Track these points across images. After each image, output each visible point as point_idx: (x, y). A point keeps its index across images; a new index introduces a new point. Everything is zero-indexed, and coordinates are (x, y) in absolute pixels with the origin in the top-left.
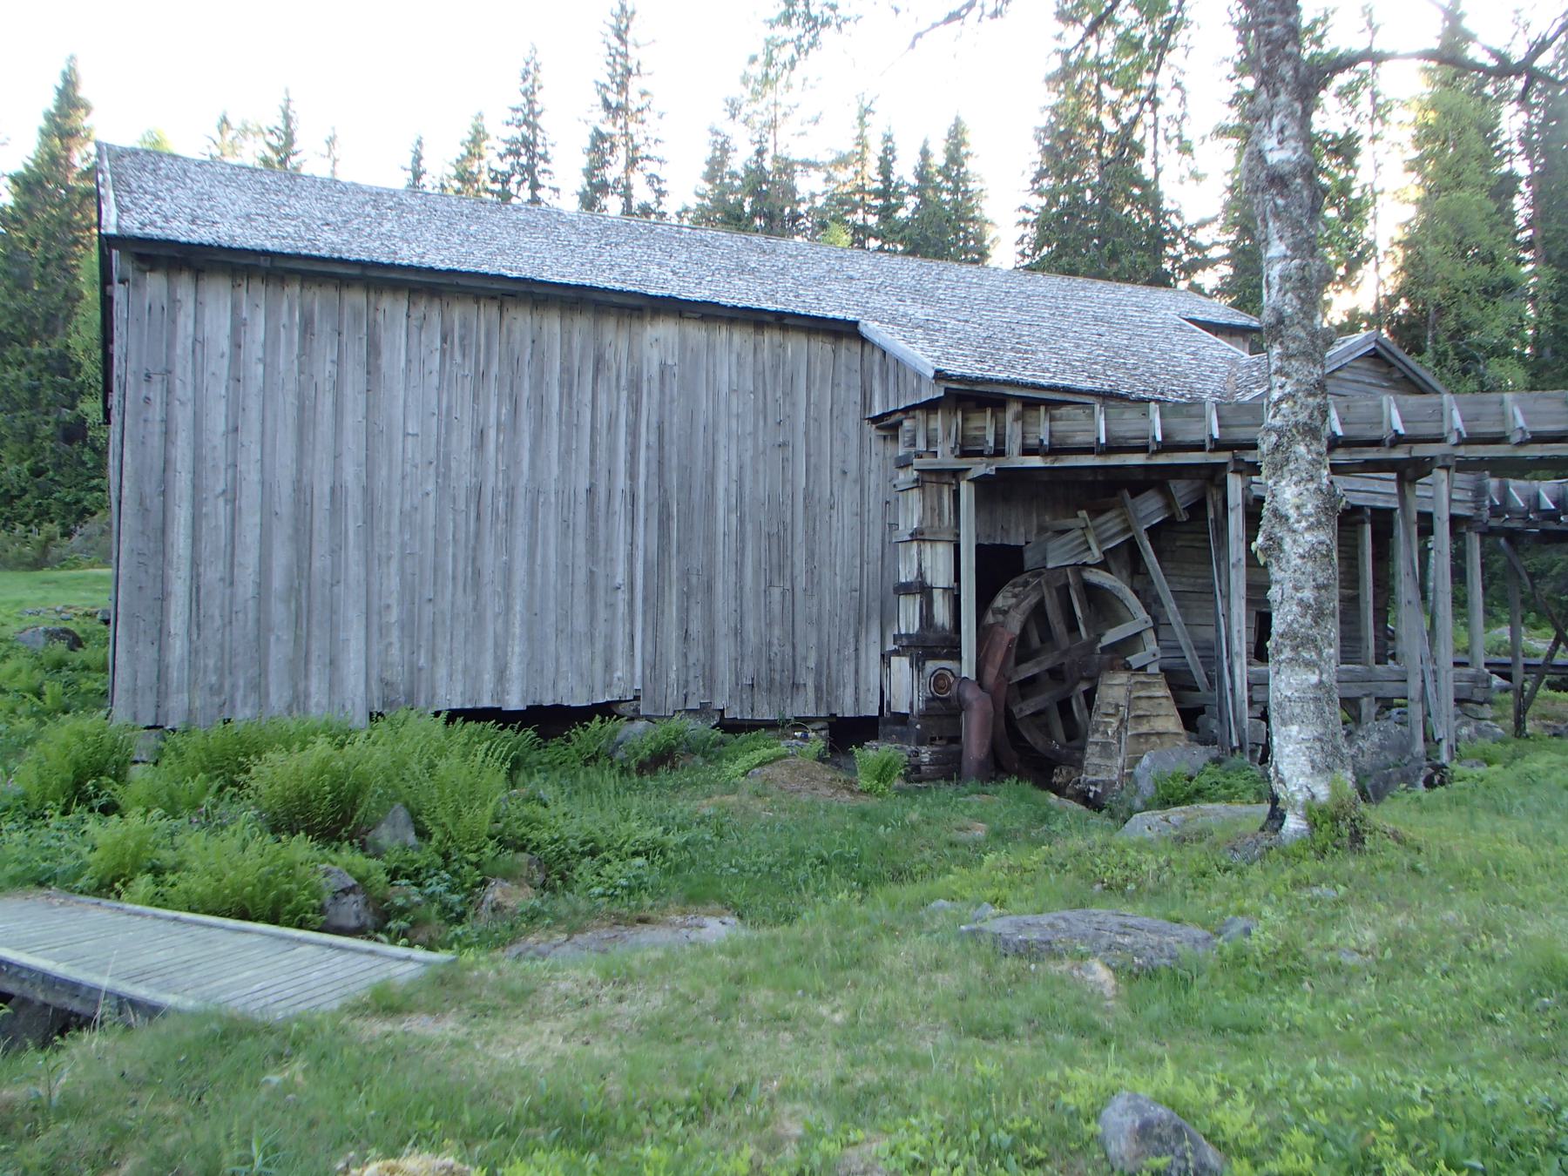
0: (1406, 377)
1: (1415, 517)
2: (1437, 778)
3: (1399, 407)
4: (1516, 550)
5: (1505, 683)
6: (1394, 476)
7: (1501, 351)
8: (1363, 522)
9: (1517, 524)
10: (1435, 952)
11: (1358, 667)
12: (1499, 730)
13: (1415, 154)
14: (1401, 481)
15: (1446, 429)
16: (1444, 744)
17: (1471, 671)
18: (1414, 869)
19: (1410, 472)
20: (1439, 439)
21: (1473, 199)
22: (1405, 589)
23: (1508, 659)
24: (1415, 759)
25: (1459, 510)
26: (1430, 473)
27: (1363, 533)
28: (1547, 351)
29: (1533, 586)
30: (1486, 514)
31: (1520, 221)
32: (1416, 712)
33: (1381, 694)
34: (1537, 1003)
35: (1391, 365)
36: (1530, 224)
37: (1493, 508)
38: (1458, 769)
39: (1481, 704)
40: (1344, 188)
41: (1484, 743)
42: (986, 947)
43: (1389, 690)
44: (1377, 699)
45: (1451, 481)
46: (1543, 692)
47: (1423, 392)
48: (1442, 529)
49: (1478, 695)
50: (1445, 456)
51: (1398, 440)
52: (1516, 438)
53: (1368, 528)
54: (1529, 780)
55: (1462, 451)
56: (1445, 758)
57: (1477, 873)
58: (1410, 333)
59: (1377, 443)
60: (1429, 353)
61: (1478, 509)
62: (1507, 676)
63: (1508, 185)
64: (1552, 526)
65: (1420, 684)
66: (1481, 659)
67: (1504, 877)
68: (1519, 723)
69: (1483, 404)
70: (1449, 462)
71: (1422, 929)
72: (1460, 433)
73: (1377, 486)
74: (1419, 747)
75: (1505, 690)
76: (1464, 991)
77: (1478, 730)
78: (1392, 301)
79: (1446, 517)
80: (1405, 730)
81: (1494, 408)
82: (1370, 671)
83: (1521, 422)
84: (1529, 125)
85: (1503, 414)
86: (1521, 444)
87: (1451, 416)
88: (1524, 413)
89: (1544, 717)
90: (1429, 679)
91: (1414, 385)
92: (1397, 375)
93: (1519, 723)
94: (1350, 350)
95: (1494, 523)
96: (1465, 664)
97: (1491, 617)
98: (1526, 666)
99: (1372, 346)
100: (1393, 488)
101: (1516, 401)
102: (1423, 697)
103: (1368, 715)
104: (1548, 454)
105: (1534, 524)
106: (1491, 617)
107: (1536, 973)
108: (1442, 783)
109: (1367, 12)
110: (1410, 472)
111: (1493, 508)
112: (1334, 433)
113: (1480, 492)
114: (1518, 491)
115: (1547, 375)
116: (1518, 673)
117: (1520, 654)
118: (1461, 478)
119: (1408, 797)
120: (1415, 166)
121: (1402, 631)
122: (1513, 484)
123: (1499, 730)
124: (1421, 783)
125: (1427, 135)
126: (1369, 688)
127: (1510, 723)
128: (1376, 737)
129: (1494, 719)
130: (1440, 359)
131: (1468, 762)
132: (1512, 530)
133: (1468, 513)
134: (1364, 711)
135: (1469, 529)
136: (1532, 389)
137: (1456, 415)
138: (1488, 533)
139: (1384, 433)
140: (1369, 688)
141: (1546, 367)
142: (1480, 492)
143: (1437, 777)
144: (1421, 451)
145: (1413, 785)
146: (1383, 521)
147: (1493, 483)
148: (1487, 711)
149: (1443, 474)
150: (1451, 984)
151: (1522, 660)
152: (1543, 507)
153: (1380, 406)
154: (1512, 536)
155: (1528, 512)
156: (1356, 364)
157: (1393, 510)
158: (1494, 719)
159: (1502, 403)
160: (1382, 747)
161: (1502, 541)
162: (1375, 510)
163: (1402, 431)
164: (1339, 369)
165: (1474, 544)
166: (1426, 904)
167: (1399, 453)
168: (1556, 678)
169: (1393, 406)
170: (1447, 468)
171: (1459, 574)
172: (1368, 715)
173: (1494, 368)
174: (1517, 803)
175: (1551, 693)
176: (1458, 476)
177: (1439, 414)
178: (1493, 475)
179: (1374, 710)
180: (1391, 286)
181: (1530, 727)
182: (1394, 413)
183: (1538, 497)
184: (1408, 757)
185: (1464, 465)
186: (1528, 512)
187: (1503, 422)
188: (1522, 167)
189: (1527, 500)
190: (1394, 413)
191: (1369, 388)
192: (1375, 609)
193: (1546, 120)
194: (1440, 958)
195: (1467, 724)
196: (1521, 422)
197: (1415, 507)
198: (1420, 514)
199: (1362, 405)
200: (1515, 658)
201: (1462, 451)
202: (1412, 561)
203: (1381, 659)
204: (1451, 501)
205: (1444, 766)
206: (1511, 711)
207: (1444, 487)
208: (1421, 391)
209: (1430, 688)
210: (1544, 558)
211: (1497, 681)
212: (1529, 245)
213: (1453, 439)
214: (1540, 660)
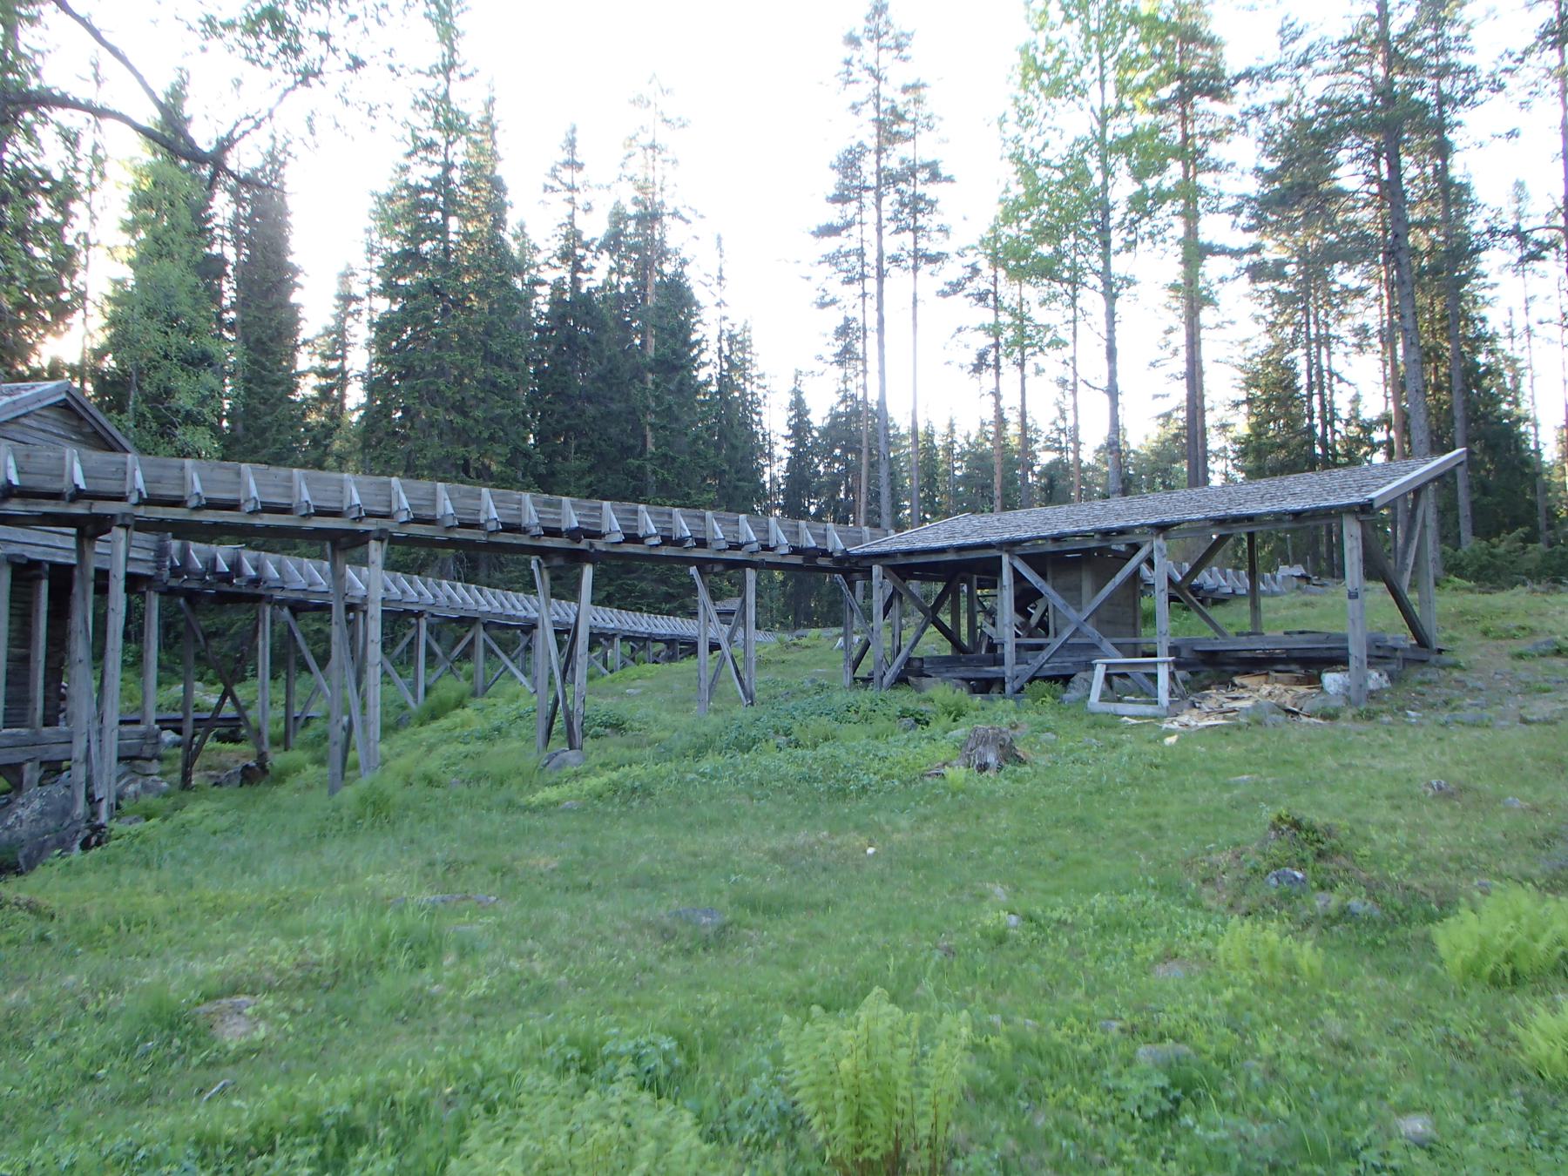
0: (96, 432)
1: (92, 573)
2: (94, 839)
3: (81, 461)
4: (194, 610)
5: (178, 738)
6: (73, 531)
7: (191, 419)
8: (40, 578)
9: (194, 585)
10: (47, 1022)
11: (23, 731)
12: (164, 784)
13: (129, 216)
14: (80, 537)
15: (127, 489)
16: (104, 804)
17: (142, 728)
18: (43, 939)
19: (91, 528)
20: (121, 498)
21: (173, 271)
22: (80, 648)
23: (179, 715)
24: (74, 822)
25: (135, 569)
26: (108, 531)
27: (38, 589)
28: (240, 425)
29: (207, 644)
30: (166, 573)
31: (226, 302)
32: (80, 772)
33: (46, 757)
34: (140, 1050)
35: (81, 418)
36: (233, 307)
37: (173, 568)
38: (116, 827)
39: (149, 760)
40: (56, 230)
41: (149, 799)
42: (1418, 911)
43: (56, 752)
44: (42, 763)
45: (129, 539)
46: (211, 744)
47: (113, 450)
48: (117, 588)
49: (148, 752)
50: (124, 515)
51: (78, 495)
52: (193, 503)
53: (45, 585)
54: (184, 829)
55: (141, 511)
56: (103, 817)
57: (108, 930)
58: (114, 389)
59: (56, 496)
60: (130, 413)
61: (158, 568)
62: (178, 731)
63: (214, 267)
64: (225, 587)
65: (85, 744)
66: (152, 716)
67: (133, 930)
68: (186, 776)
69: (164, 466)
70: (128, 521)
71: (37, 1001)
72: (140, 493)
73: (58, 541)
74: (81, 808)
75: (177, 745)
76: (70, 1056)
77: (145, 788)
78: (99, 354)
79: (121, 575)
80: (69, 793)
81: (176, 472)
82: (37, 734)
83: (198, 488)
84: (237, 215)
85: (183, 478)
86: (197, 509)
87: (134, 476)
88: (201, 480)
89: (209, 768)
90: (94, 738)
91: (104, 442)
92: (88, 430)
93: (186, 776)
94: (39, 398)
95: (174, 583)
96: (137, 722)
97: (168, 672)
98: (196, 720)
99: (64, 396)
100: (71, 543)
101: (195, 468)
102: (87, 759)
103: (30, 781)
104: (220, 520)
105: (211, 585)
106: (168, 672)
107: (144, 1020)
108: (98, 843)
109: (1519, 185)
110: (89, 529)
111: (173, 568)
112: (9, 482)
113: (162, 552)
114: (198, 553)
115: (238, 448)
116: (188, 727)
117: (191, 710)
118: (140, 537)
119: (60, 863)
120: (130, 228)
121: (73, 691)
122: (193, 546)
123: (164, 784)
124: (77, 846)
125: (141, 201)
126: (36, 751)
127: (177, 776)
128: (37, 804)
129: (161, 774)
130: (140, 419)
131: (128, 819)
132: (191, 590)
133: (150, 573)
134: (26, 777)
135: (149, 588)
136: (224, 458)
137: (139, 474)
138: (168, 593)
139: (64, 486)
140: (36, 751)
141: (237, 440)
142: (162, 552)
143: (95, 837)
144: (101, 507)
145: (69, 849)
146: (62, 577)
147: (175, 545)
148: (155, 767)
149: (121, 532)
150: (58, 1052)
151: (193, 715)
152: (219, 569)
153: (63, 458)
154: (192, 596)
155: (204, 574)
156: (44, 413)
157: (72, 566)
158: (161, 774)
159: (182, 468)
160: (42, 813)
161: (182, 601)
162: (53, 565)
163: (83, 486)
164: (24, 415)
165: (154, 602)
166: (47, 973)
167: (79, 509)
168: (225, 731)
169: (76, 459)
170: (127, 527)
171: (133, 633)
172: (30, 781)
173: (184, 435)
174: (166, 854)
175: (218, 745)
176: (136, 534)
177: (123, 473)
178: (175, 537)
179: (37, 775)
180: (101, 338)
181: (196, 778)
182: (77, 467)
183: (215, 560)
184: (68, 822)
185: (143, 526)
186: (204, 574)
187: (183, 486)
188: (230, 253)
189: (205, 563)
190: (77, 467)
191: (57, 439)
192: (47, 668)
193: (255, 213)
194: (50, 1027)
195: (133, 781)
196: (198, 488)
197: (93, 563)
198: (97, 571)
199: (44, 455)
200: (186, 713)
201: (141, 511)
202: (86, 622)
203: (50, 721)
204: (128, 559)
205: (102, 826)
206: (179, 764)
207: (122, 546)
208: (111, 448)
209: (94, 749)
210: (225, 618)
211: (168, 736)
212: (231, 327)
213: (134, 498)
214: (207, 715)
